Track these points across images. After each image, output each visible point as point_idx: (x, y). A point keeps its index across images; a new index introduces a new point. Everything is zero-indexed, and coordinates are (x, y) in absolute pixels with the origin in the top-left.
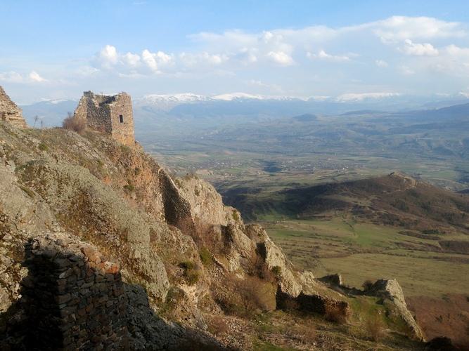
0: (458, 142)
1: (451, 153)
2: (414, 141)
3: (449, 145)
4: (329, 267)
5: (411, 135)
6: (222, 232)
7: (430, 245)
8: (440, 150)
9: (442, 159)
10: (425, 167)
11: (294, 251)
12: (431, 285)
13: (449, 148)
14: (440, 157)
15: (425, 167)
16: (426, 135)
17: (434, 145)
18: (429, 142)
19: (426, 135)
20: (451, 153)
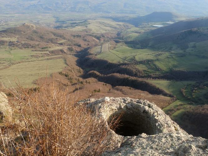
9: (48, 13)
10: (41, 17)
13: (50, 7)
15: (41, 17)
20: (51, 10)
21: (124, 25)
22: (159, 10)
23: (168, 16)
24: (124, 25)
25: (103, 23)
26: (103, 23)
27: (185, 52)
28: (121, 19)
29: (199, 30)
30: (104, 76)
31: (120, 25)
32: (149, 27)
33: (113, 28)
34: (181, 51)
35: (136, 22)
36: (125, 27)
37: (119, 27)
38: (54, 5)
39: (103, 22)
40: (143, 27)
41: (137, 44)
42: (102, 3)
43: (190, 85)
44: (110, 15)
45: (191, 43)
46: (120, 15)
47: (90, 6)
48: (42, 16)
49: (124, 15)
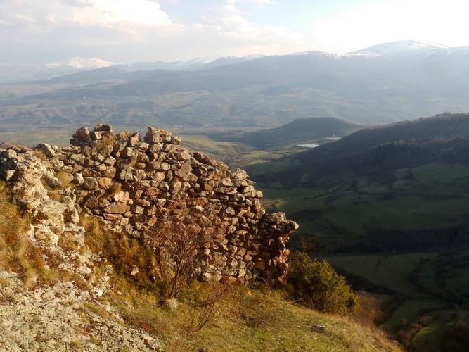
0: (72, 110)
1: (66, 121)
2: (29, 112)
3: (65, 114)
4: (316, 336)
5: (25, 106)
6: (207, 64)
7: (222, 146)
8: (57, 119)
9: (60, 128)
10: (44, 137)
11: (137, 185)
12: (121, 81)
13: (64, 117)
14: (58, 126)
15: (44, 137)
16: (41, 105)
17: (51, 115)
18: (44, 112)
19: (41, 105)
20: (66, 121)
21: (234, 147)
22: (306, 114)
23: (328, 124)
24: (234, 147)
25: (189, 144)
26: (189, 144)
27: (391, 188)
28: (228, 136)
29: (409, 144)
30: (94, 163)
31: (226, 147)
32: (291, 149)
33: (213, 153)
34: (382, 189)
35: (259, 140)
36: (236, 150)
37: (225, 151)
38: (75, 111)
39: (189, 142)
40: (277, 150)
41: (274, 182)
42: (183, 107)
43: (427, 260)
44: (201, 130)
45: (399, 170)
46: (222, 129)
47: (155, 112)
48: (45, 134)
49: (231, 129)
